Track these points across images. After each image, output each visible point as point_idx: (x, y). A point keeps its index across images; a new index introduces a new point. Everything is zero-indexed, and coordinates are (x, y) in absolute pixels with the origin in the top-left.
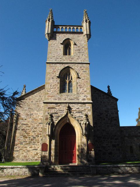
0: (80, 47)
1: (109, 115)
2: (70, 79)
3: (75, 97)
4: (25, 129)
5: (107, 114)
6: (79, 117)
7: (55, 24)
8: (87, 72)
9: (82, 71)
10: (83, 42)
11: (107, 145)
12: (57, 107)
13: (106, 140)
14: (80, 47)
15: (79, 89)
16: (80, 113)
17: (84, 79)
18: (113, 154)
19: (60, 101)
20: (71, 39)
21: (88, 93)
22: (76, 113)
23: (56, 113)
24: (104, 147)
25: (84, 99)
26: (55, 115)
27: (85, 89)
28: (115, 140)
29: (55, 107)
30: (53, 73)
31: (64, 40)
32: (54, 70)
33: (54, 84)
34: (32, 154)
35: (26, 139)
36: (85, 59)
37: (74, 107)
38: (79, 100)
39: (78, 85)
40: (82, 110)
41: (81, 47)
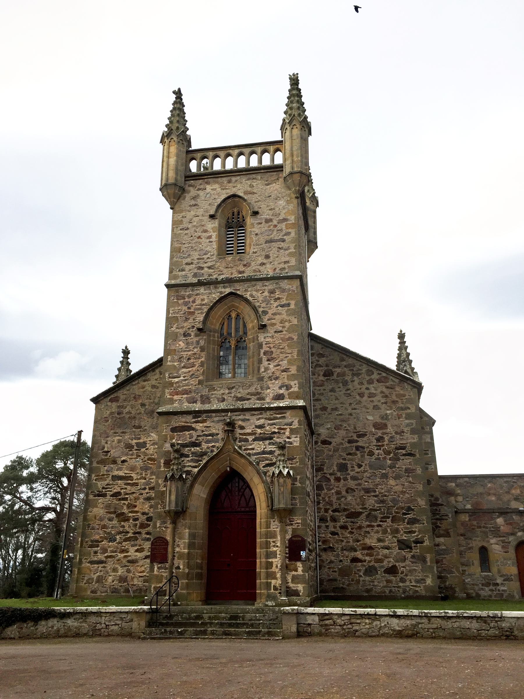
0: (271, 220)
1: (386, 438)
2: (241, 333)
3: (252, 390)
4: (122, 491)
5: (380, 434)
6: (264, 452)
7: (194, 147)
8: (292, 306)
9: (276, 304)
10: (282, 203)
11: (379, 540)
12: (199, 426)
13: (375, 524)
14: (271, 220)
15: (265, 363)
16: (267, 442)
17: (281, 329)
18: (402, 573)
19: (207, 407)
20: (241, 194)
21: (292, 377)
22: (254, 440)
24: (370, 548)
25: (280, 397)
26: (193, 449)
27: (284, 364)
28: (408, 524)
29: (193, 425)
30: (187, 319)
31: (219, 201)
32: (189, 308)
33: (190, 353)
34: (143, 572)
35: (126, 524)
36: (285, 262)
37: (251, 424)
38: (263, 399)
39: (262, 351)
40: (273, 430)
41: (275, 222)
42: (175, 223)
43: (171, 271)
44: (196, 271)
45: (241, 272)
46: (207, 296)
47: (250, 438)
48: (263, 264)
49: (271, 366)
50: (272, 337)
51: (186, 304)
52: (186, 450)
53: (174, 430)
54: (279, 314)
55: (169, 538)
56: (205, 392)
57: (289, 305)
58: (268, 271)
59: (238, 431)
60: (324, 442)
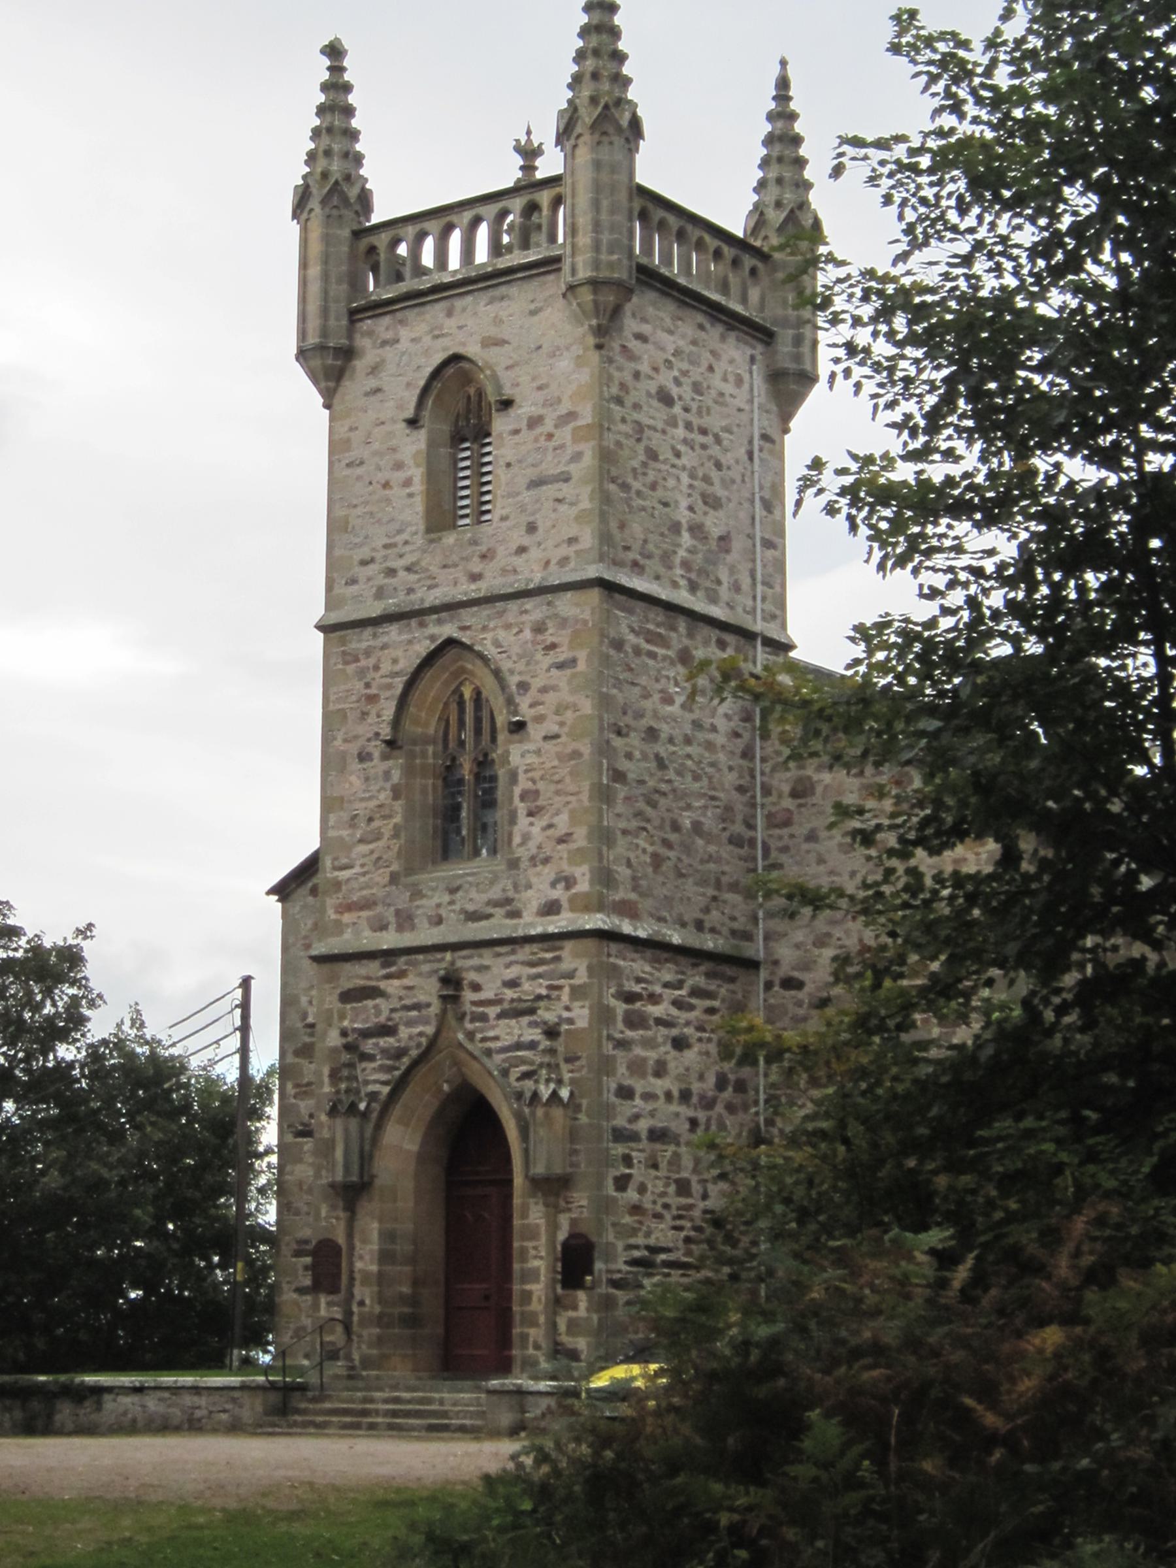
6: (518, 1046)
8: (582, 666)
15: (523, 821)
19: (408, 939)
21: (578, 856)
23: (387, 1030)
27: (562, 822)
30: (364, 714)
42: (337, 447)
43: (329, 588)
44: (381, 580)
45: (475, 577)
46: (405, 648)
47: (492, 1011)
48: (522, 550)
49: (535, 830)
50: (538, 752)
51: (361, 673)
52: (369, 1046)
53: (347, 996)
54: (554, 688)
55: (341, 1240)
56: (402, 899)
57: (573, 662)
58: (531, 573)
59: (468, 996)
60: (790, 983)
